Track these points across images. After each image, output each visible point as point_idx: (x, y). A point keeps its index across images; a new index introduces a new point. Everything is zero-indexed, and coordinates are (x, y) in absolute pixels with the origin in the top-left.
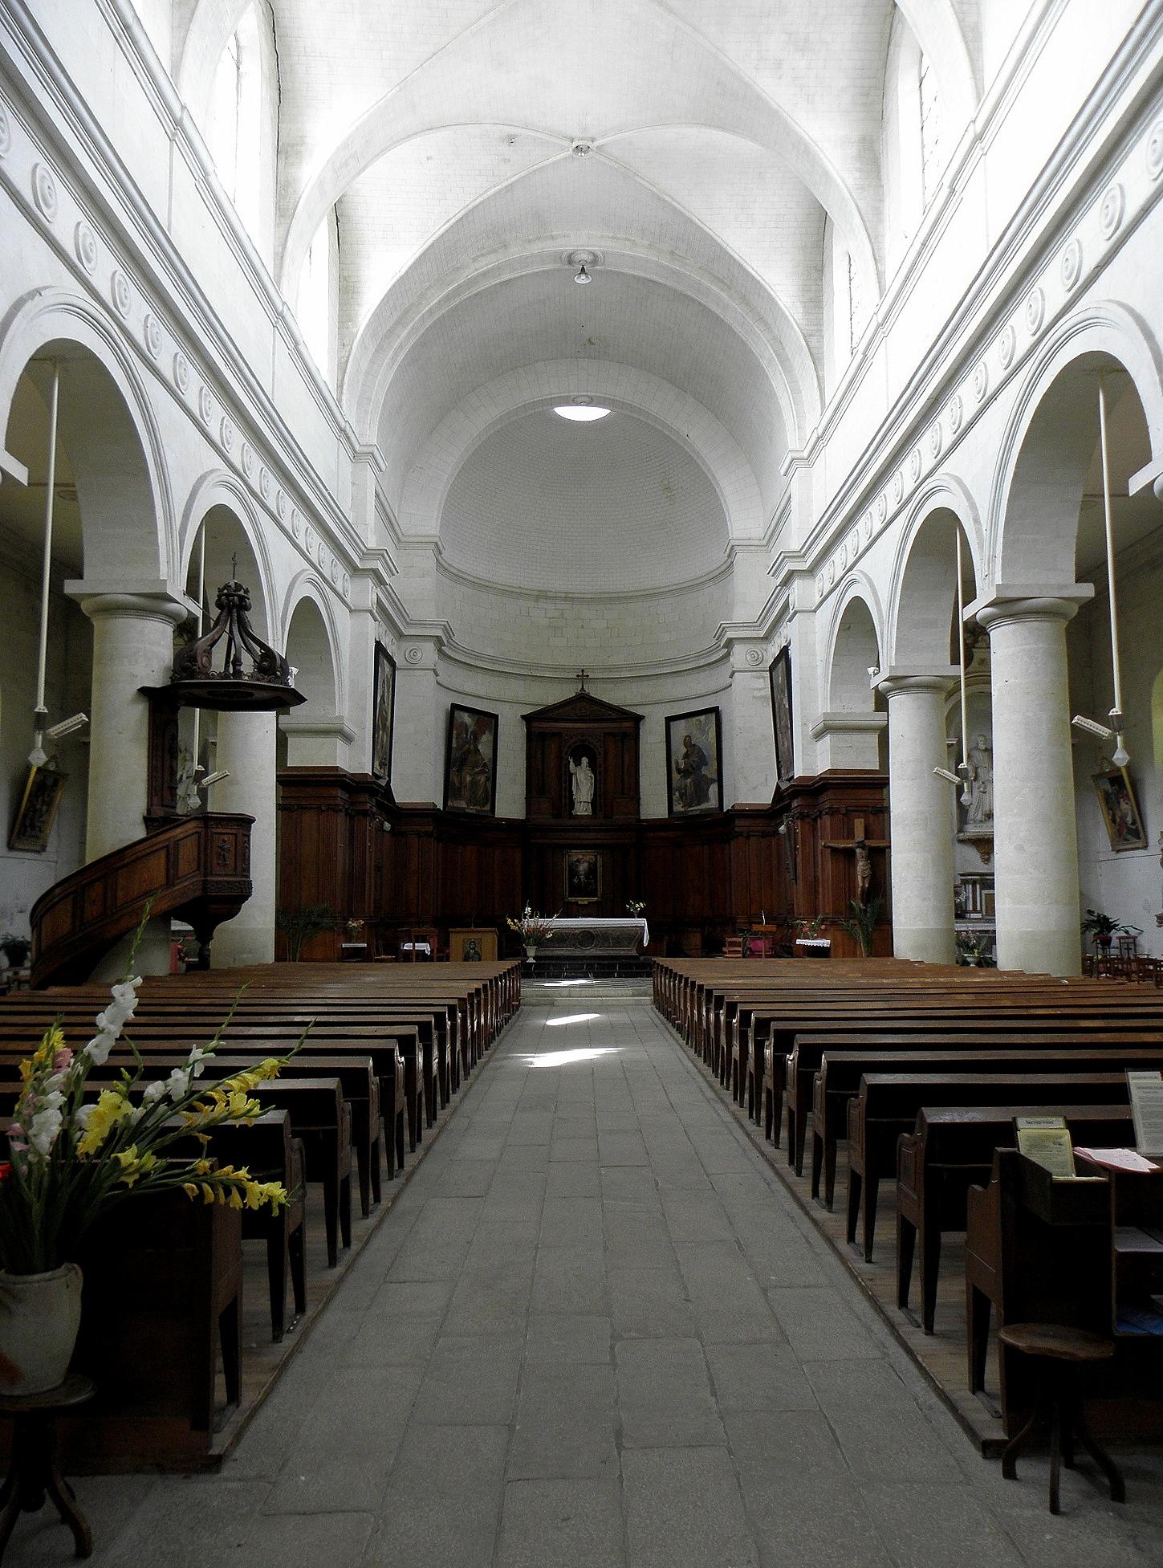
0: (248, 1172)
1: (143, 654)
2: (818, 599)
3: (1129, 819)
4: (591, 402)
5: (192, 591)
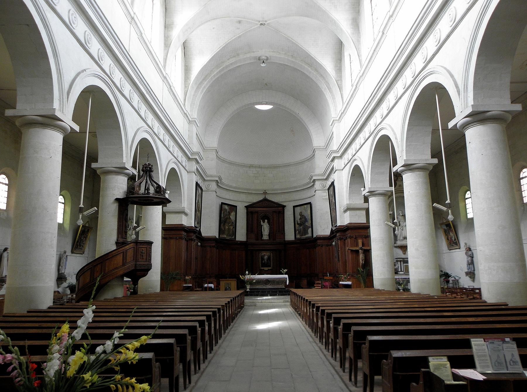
0: (136, 380)
1: (117, 187)
2: (343, 166)
3: (453, 239)
4: (267, 104)
5: (134, 166)
